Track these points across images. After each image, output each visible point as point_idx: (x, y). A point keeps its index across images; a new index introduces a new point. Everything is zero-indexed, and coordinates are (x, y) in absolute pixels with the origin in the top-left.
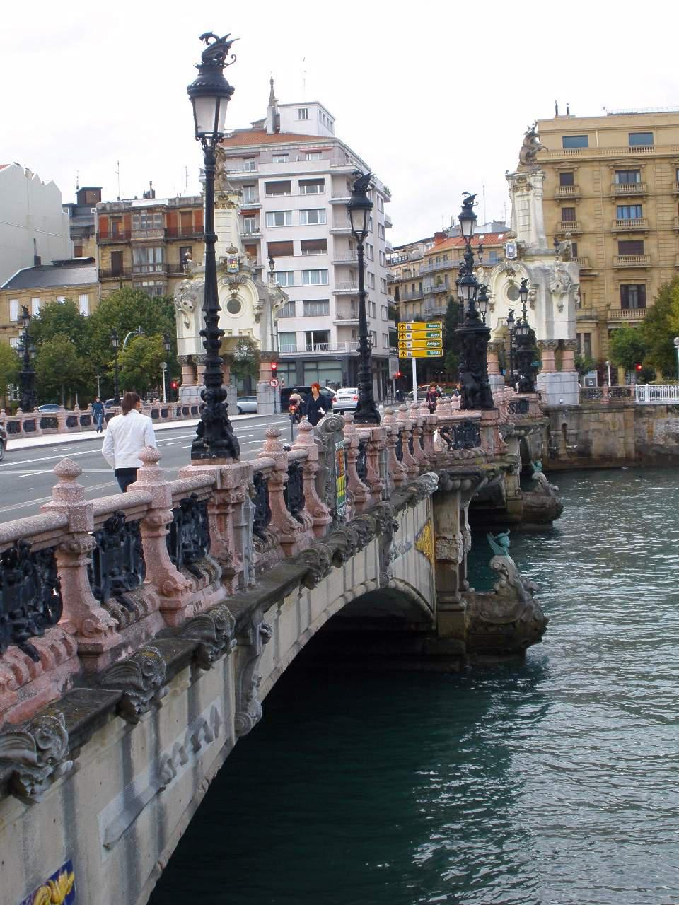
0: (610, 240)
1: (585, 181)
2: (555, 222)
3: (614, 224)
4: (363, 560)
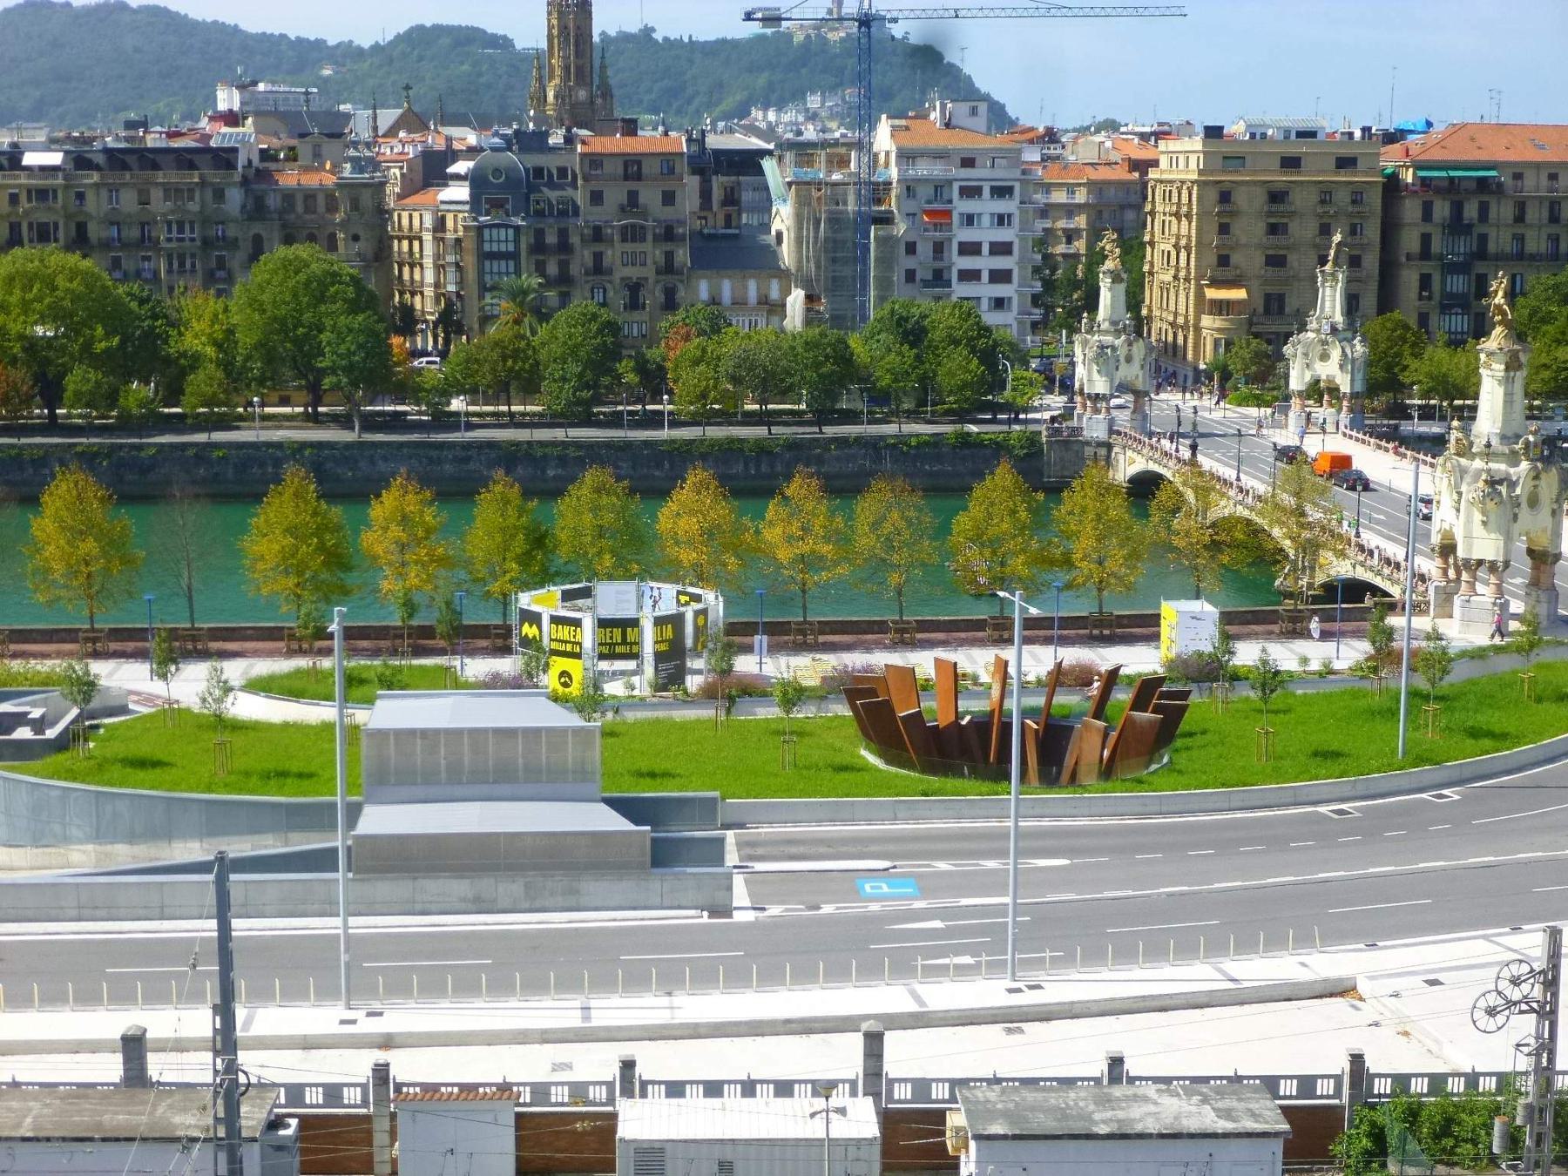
1: (1240, 199)
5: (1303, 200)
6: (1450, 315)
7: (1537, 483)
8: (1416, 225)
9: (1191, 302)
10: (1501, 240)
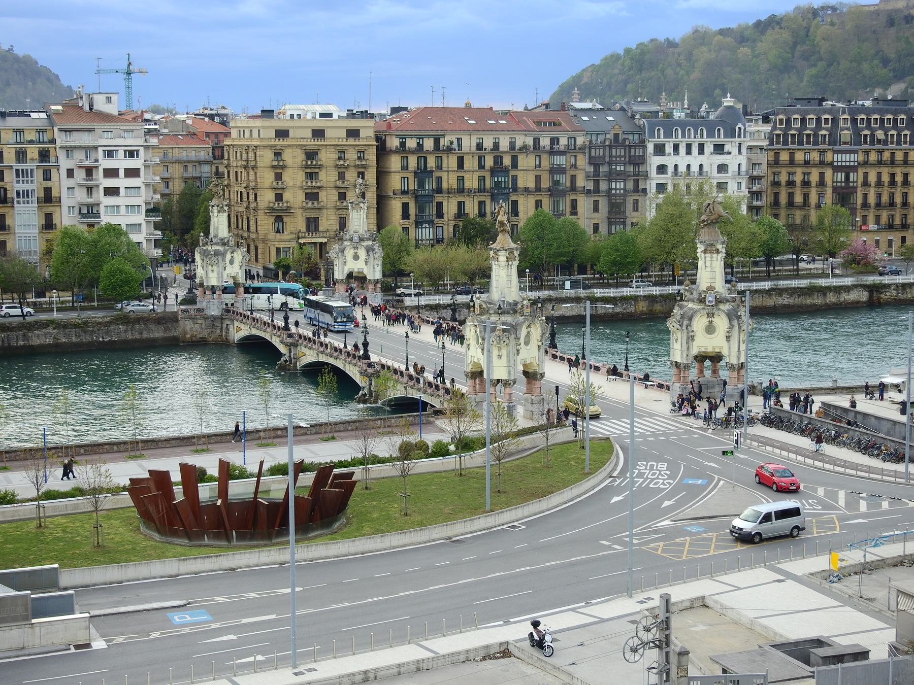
0: (301, 192)
1: (287, 156)
2: (271, 181)
3: (304, 183)
4: (185, 430)
5: (327, 157)
6: (422, 228)
7: (529, 329)
8: (399, 172)
9: (510, 207)
10: (449, 181)
